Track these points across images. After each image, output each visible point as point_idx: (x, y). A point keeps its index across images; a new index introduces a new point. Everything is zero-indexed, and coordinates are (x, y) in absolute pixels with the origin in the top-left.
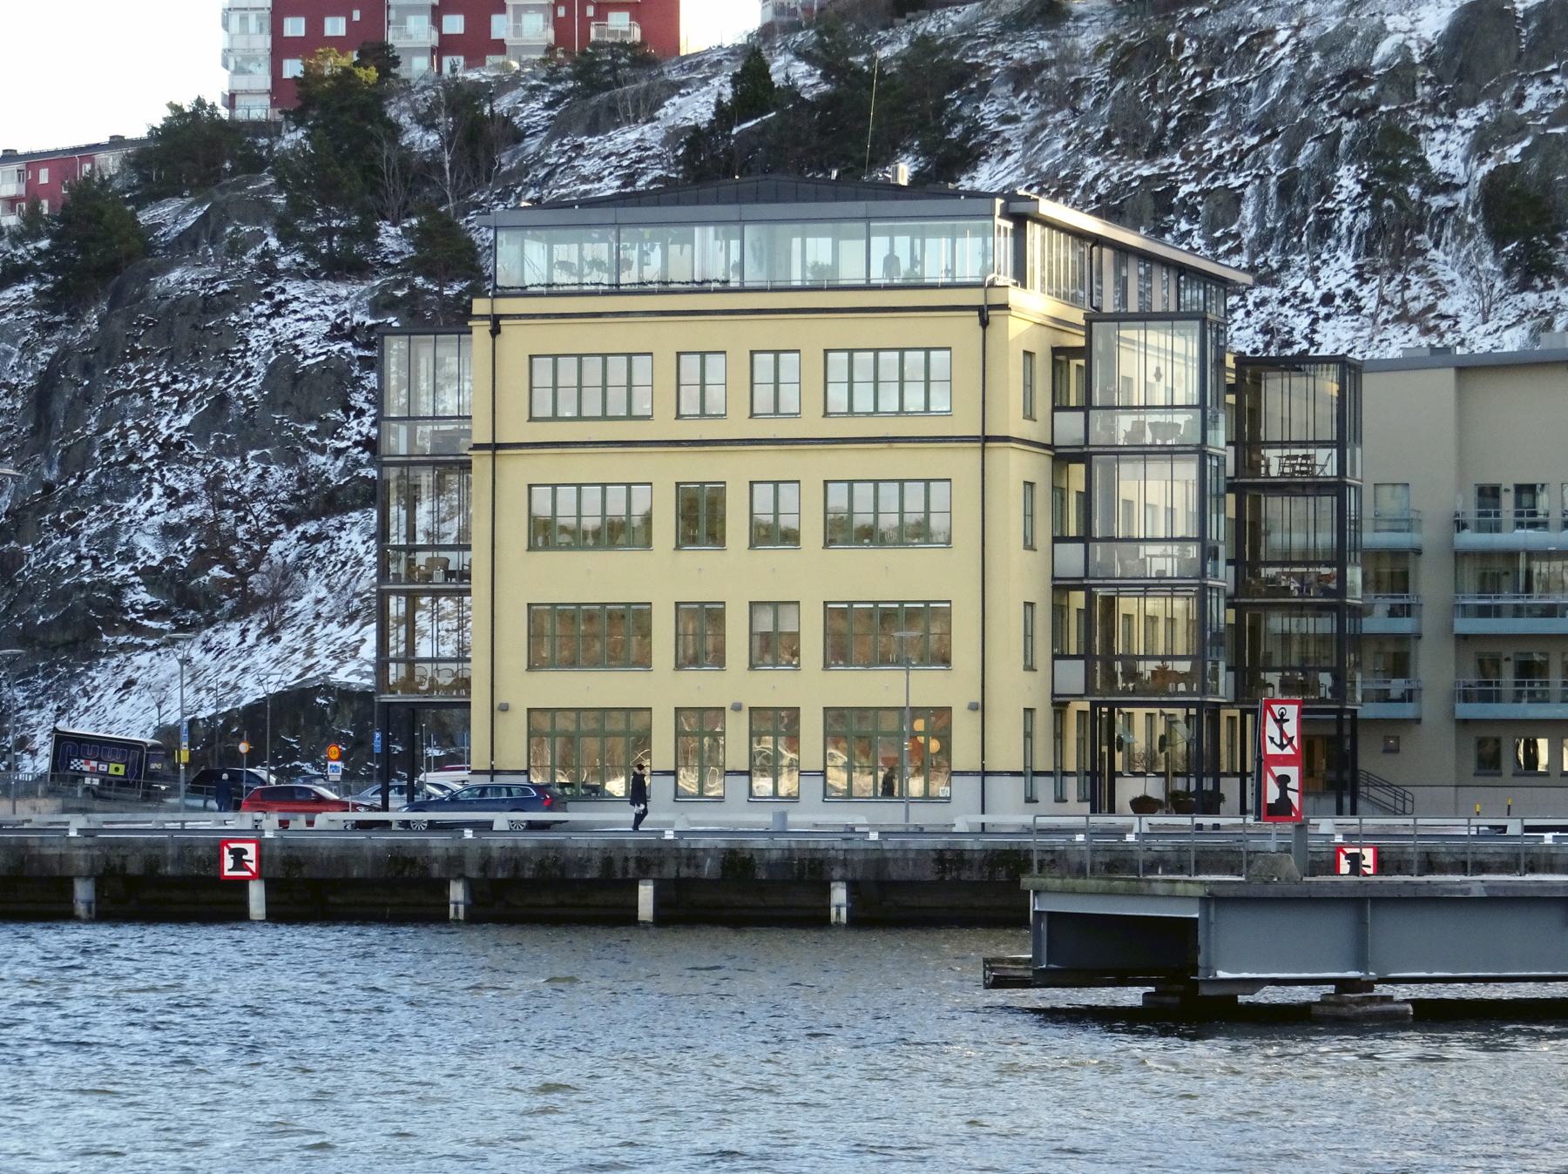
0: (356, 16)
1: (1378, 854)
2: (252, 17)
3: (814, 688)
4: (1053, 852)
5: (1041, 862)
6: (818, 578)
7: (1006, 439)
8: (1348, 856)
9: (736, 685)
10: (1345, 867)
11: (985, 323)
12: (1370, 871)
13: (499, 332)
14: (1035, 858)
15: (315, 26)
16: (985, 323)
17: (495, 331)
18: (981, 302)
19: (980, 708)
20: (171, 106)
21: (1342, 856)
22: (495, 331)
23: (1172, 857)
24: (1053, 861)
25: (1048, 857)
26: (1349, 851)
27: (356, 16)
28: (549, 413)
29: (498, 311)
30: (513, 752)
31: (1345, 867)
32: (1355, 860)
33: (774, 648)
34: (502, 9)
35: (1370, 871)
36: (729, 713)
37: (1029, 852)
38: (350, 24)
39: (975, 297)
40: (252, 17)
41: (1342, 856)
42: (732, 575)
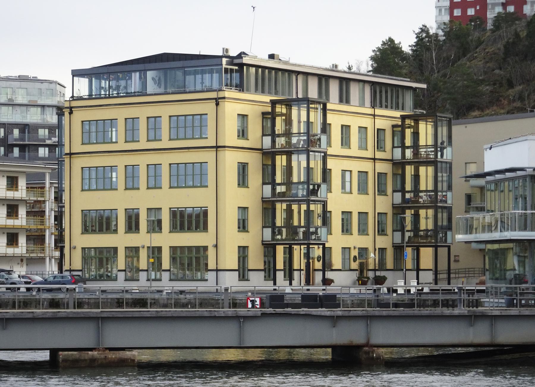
0: (478, 8)
1: (261, 300)
2: (443, 10)
3: (168, 239)
4: (154, 299)
5: (151, 303)
6: (169, 199)
7: (224, 147)
8: (251, 301)
9: (142, 239)
10: (250, 305)
11: (217, 104)
12: (258, 307)
13: (72, 113)
14: (149, 302)
15: (464, 12)
16: (217, 104)
17: (71, 113)
18: (216, 97)
19: (216, 246)
20: (400, 43)
21: (249, 301)
22: (71, 113)
23: (193, 301)
24: (155, 303)
25: (153, 301)
26: (251, 299)
27: (478, 8)
28: (102, 141)
29: (72, 105)
30: (77, 264)
31: (250, 305)
32: (253, 302)
33: (156, 226)
34: (526, 3)
35: (258, 307)
36: (141, 249)
37: (147, 299)
38: (476, 11)
39: (213, 95)
40: (443, 10)
41: (249, 301)
42: (142, 200)
